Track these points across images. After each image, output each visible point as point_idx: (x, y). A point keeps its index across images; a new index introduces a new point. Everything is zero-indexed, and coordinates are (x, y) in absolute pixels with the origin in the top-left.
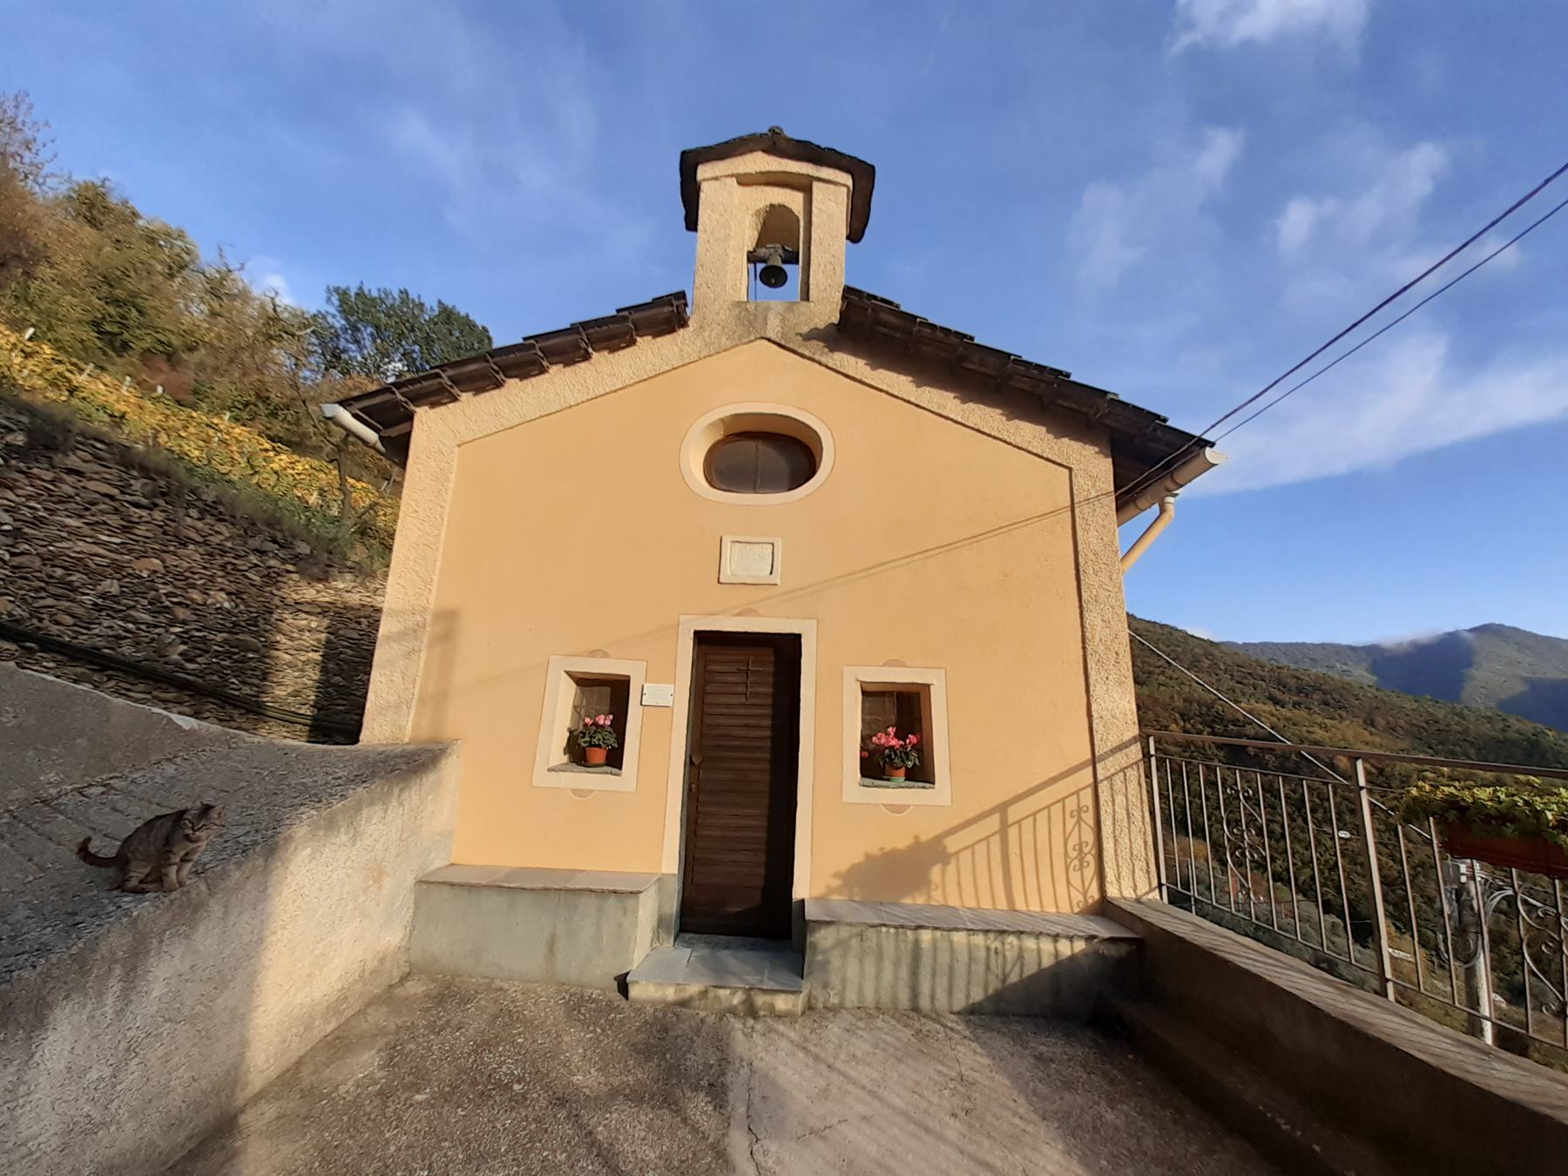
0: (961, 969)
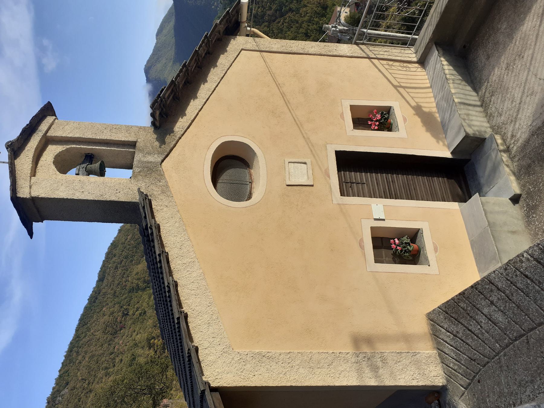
0: (462, 91)
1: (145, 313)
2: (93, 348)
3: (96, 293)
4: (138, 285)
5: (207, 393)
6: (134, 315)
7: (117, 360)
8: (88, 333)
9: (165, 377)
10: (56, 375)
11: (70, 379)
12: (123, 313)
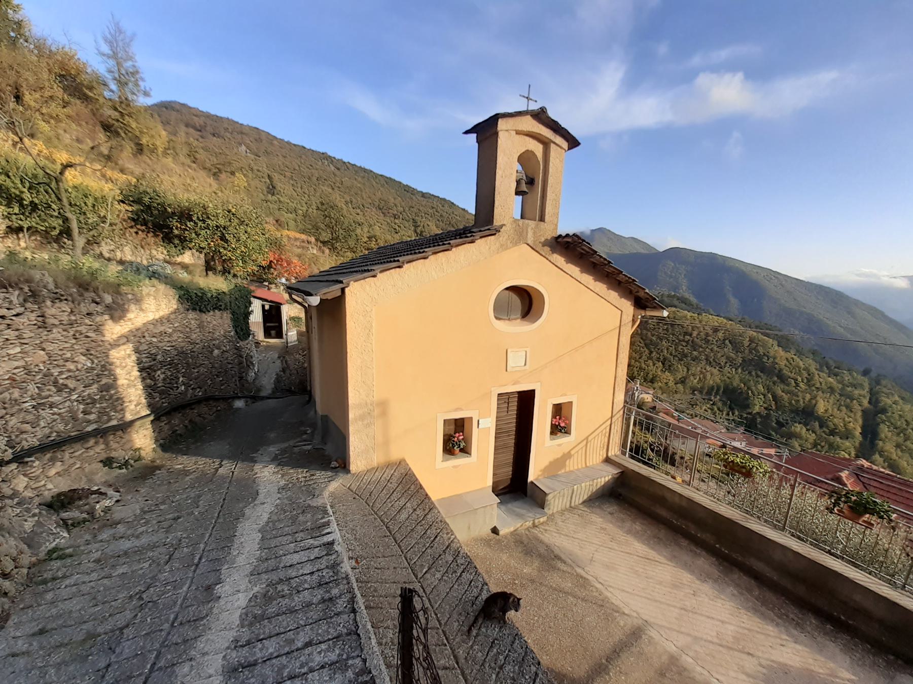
5: (341, 286)
10: (346, 160)
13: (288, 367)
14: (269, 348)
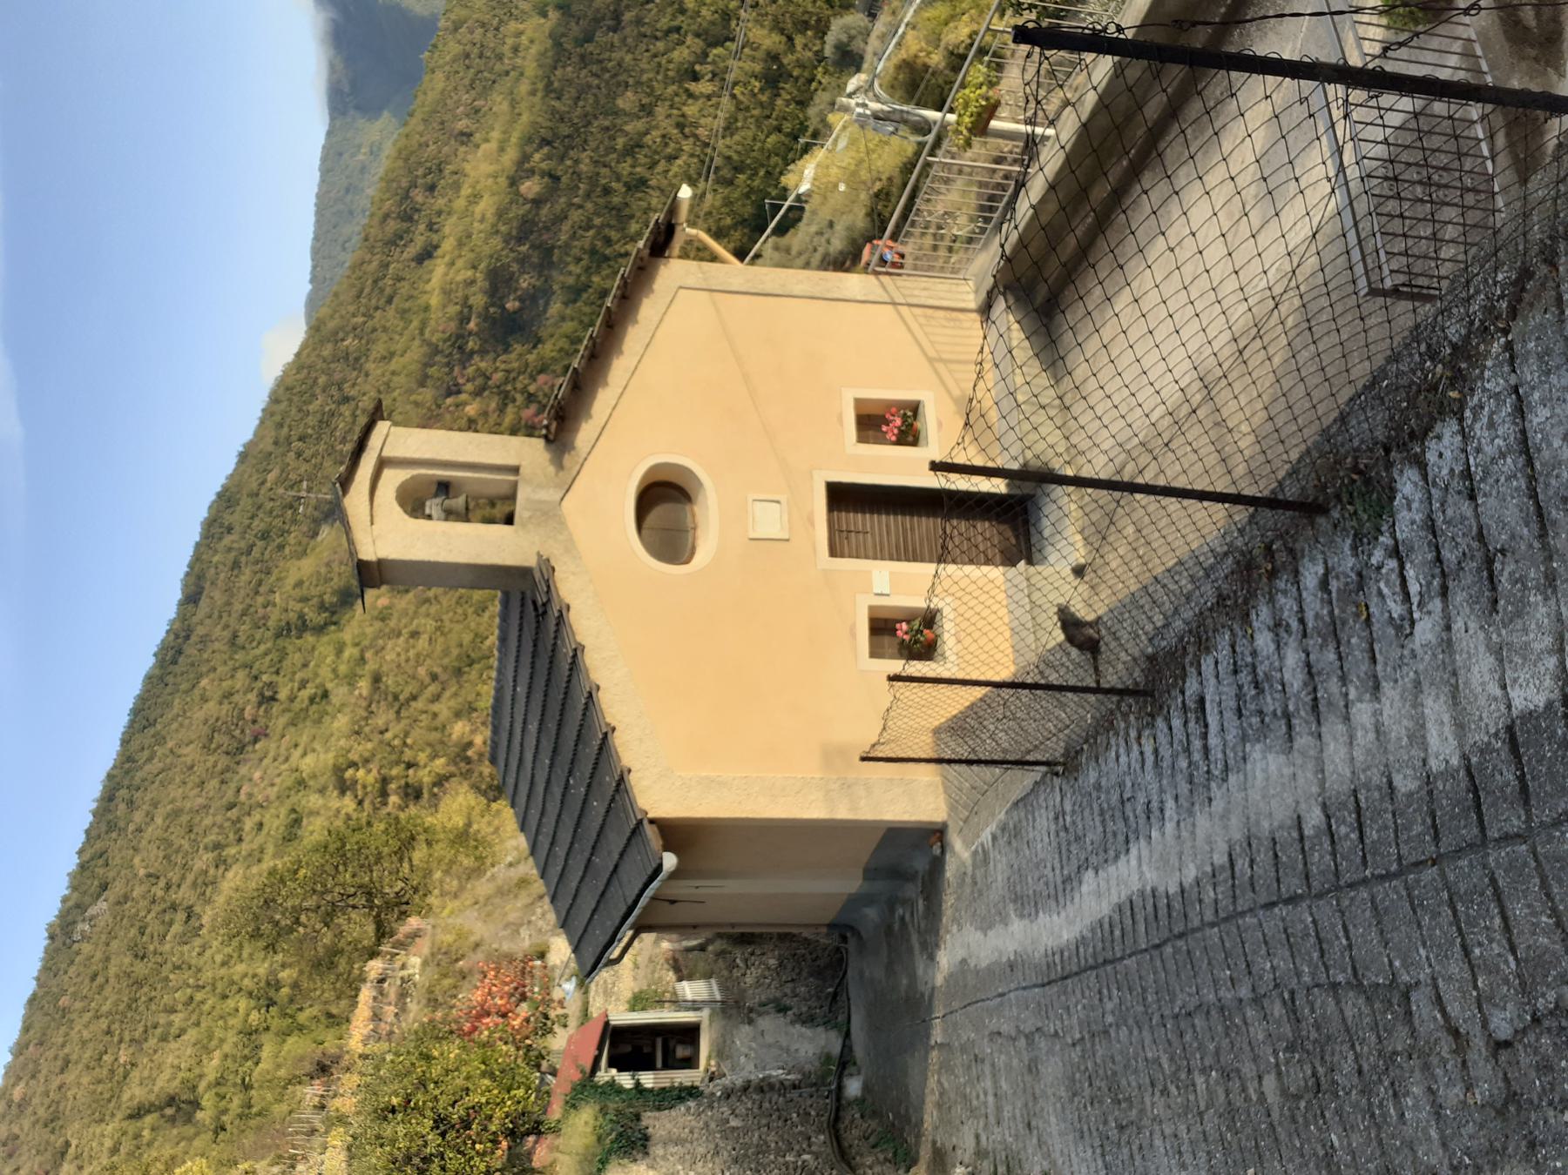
1: (325, 695)
2: (175, 792)
3: (177, 636)
4: (301, 616)
5: (645, 822)
6: (292, 699)
7: (248, 824)
8: (160, 751)
9: (406, 865)
10: (73, 862)
11: (111, 874)
12: (261, 694)
13: (776, 1001)
14: (721, 1052)
